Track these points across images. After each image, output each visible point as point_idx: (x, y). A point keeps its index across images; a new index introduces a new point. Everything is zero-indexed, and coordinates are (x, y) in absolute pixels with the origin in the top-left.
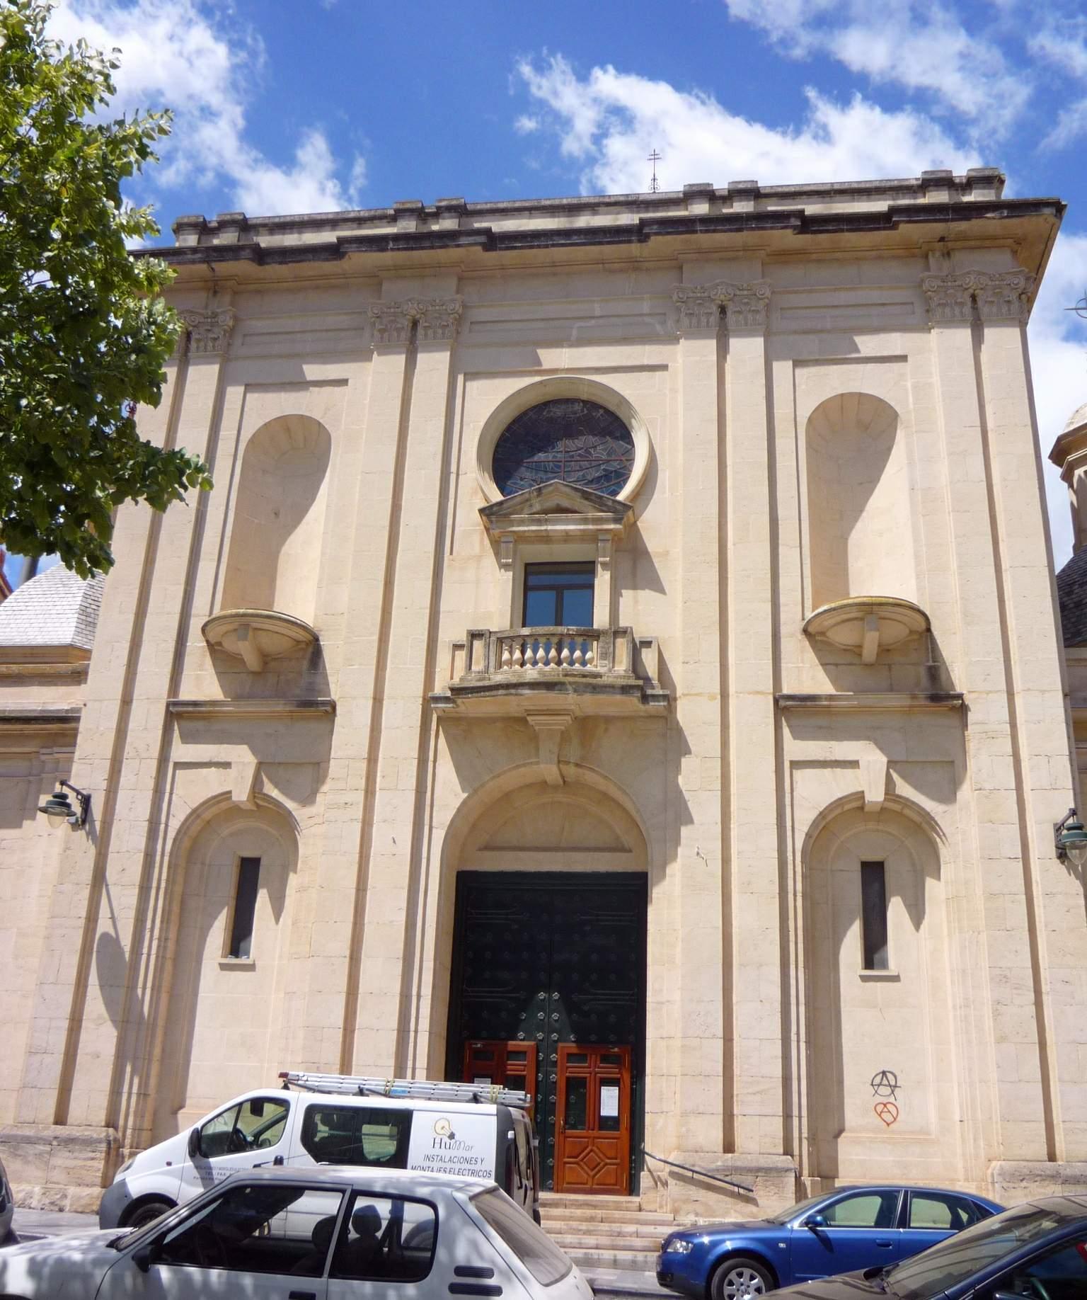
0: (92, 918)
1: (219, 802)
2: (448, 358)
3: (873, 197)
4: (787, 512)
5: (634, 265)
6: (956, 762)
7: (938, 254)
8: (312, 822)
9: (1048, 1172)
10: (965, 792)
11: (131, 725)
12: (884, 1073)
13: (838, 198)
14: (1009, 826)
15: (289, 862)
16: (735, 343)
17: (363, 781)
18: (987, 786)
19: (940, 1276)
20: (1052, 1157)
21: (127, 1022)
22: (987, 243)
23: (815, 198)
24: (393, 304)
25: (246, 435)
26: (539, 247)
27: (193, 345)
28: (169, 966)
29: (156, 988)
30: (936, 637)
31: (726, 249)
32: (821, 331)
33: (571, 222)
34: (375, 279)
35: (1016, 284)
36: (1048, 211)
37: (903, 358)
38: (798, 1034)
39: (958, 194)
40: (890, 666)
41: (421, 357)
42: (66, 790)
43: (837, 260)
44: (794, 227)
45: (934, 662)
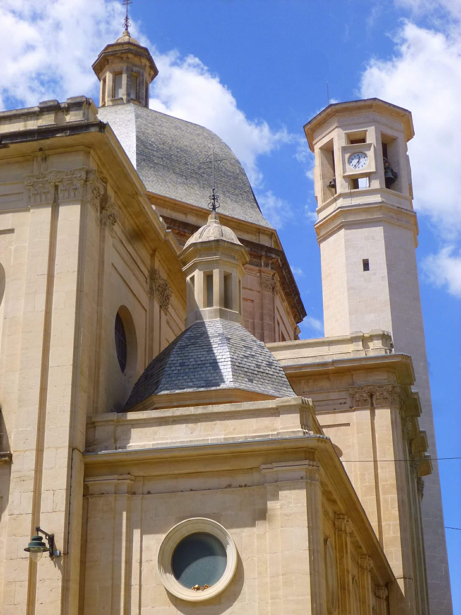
3: (12, 121)
6: (4, 497)
7: (39, 159)
14: (24, 537)
16: (63, 210)
22: (69, 149)
24: (69, 172)
27: (61, 195)
30: (4, 416)
35: (80, 177)
36: (93, 130)
37: (11, 231)
39: (63, 115)
42: (40, 534)
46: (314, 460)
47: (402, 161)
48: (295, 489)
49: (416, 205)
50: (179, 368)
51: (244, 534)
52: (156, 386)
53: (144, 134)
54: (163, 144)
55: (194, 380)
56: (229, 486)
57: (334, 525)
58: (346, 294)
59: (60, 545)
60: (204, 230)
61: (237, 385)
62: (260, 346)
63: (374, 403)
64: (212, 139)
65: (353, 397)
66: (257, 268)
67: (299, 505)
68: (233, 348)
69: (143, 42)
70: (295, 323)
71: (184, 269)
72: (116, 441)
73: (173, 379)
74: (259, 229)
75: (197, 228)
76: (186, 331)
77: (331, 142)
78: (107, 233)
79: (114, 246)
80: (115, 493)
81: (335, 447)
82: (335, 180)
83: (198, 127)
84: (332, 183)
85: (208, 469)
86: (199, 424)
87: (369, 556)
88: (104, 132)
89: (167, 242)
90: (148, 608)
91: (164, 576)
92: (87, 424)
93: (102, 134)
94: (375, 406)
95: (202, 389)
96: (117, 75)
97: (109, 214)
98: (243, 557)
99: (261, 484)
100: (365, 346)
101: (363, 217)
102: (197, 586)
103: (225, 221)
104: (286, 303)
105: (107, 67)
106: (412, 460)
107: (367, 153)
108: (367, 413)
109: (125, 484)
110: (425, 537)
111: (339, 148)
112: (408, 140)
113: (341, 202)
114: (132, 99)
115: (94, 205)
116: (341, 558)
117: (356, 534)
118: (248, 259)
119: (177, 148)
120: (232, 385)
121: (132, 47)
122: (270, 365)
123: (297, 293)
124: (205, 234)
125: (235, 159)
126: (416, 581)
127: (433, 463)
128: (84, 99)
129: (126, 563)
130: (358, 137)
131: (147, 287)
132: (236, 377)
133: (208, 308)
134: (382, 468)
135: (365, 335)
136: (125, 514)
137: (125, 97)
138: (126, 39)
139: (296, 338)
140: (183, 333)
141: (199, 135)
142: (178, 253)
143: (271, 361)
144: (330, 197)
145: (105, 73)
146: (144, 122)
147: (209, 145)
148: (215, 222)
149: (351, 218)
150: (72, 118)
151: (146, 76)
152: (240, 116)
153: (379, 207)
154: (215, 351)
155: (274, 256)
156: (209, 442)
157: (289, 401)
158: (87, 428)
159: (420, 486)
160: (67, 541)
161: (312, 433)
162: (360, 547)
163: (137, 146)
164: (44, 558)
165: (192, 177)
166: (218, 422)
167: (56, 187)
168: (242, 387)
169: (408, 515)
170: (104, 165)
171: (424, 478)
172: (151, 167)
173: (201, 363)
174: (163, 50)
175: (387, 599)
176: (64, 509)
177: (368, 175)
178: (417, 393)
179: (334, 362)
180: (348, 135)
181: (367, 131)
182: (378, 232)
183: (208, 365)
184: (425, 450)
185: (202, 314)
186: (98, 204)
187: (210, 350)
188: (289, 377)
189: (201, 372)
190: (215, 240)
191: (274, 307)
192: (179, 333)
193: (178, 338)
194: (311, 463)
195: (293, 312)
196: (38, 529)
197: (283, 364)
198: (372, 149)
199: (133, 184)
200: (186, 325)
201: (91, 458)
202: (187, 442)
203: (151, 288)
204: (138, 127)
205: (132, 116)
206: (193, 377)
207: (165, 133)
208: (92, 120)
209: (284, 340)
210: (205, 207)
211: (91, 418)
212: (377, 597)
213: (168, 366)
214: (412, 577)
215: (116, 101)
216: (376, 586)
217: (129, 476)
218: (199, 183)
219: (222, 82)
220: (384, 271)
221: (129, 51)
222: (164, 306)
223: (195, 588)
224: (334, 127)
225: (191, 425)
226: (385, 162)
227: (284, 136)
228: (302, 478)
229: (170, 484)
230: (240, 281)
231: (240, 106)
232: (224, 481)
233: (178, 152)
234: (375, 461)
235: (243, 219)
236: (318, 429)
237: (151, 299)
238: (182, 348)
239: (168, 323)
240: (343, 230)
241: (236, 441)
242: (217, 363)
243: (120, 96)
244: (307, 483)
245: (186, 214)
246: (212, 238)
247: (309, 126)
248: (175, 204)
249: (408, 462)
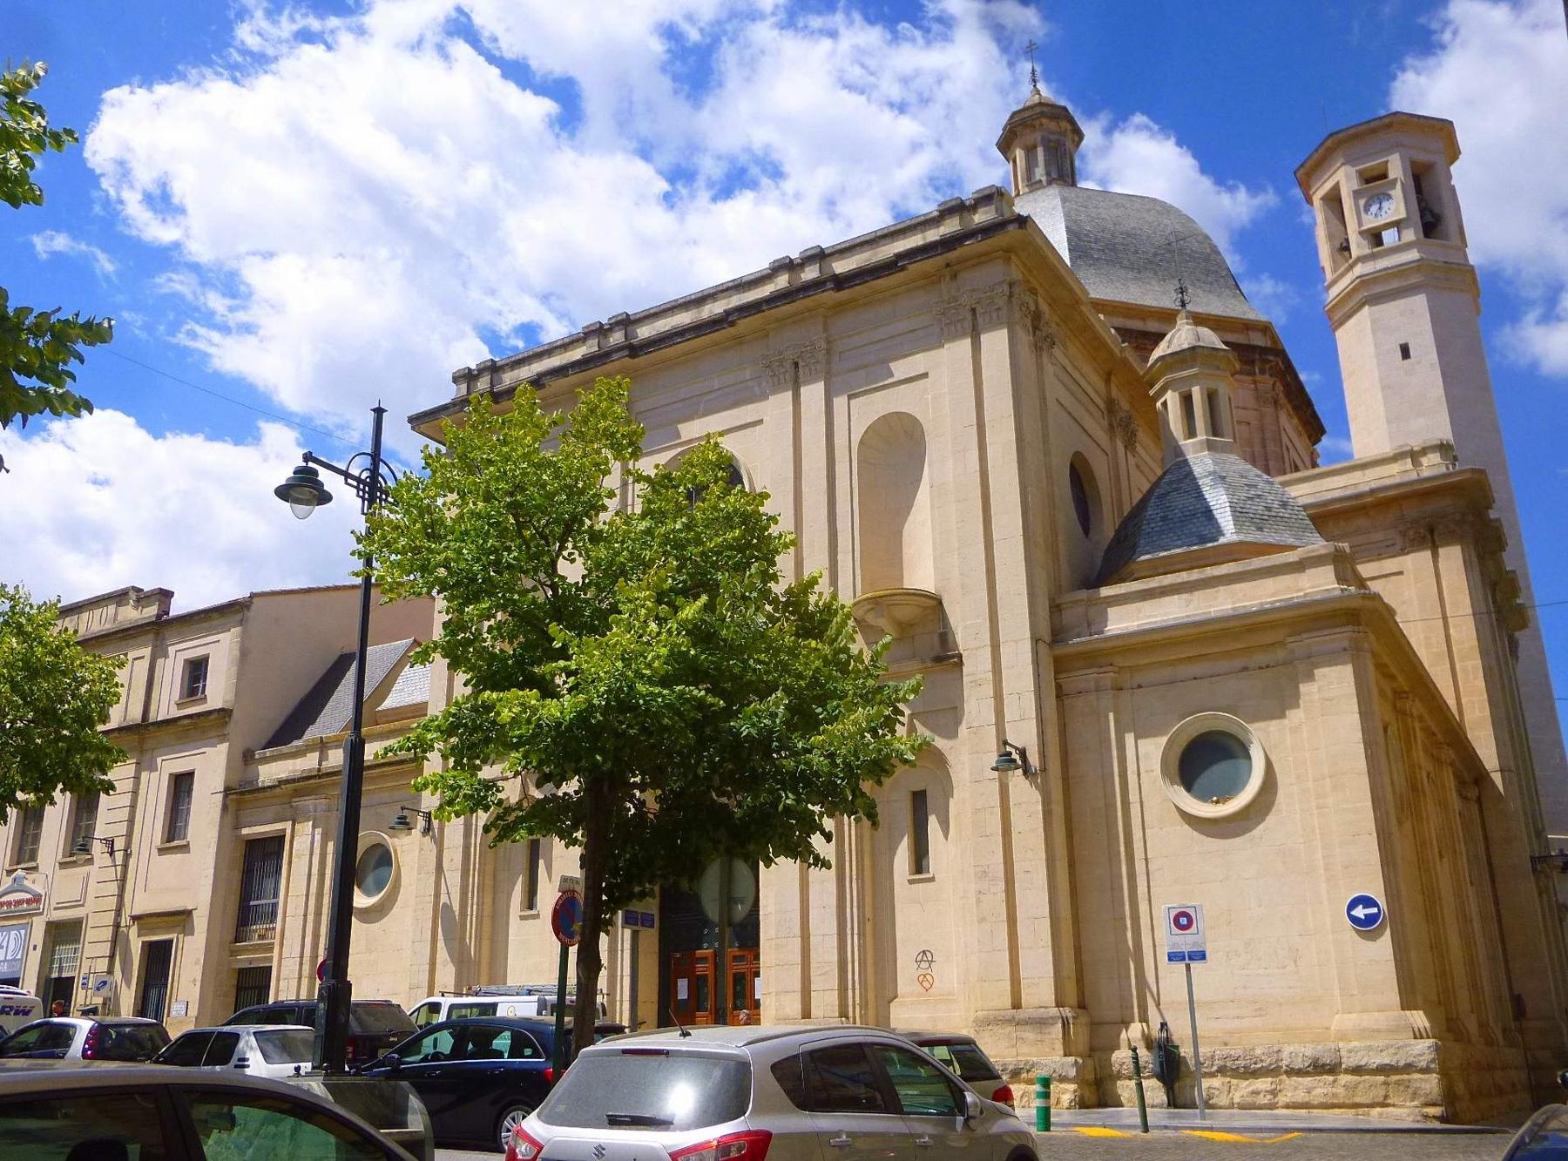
0: (437, 895)
2: (791, 398)
4: (843, 524)
5: (739, 341)
9: (1007, 1018)
10: (963, 730)
12: (924, 952)
13: (883, 242)
15: (947, 791)
16: (985, 338)
18: (975, 724)
20: (1016, 1005)
21: (462, 962)
23: (866, 247)
25: (856, 439)
26: (666, 347)
27: (980, 320)
28: (487, 921)
29: (479, 938)
31: (796, 314)
32: (866, 366)
34: (763, 334)
36: (1011, 228)
37: (925, 375)
38: (852, 929)
40: (913, 637)
41: (984, 338)
42: (1009, 749)
43: (879, 300)
44: (832, 289)
46: (1359, 624)
47: (1445, 194)
48: (1337, 665)
49: (1473, 258)
50: (1161, 523)
51: (1272, 729)
52: (1133, 550)
54: (1103, 231)
56: (1245, 669)
57: (1395, 707)
58: (1380, 396)
59: (1034, 760)
60: (1173, 336)
61: (1242, 537)
62: (1268, 482)
65: (1405, 536)
66: (1249, 378)
68: (1231, 489)
69: (1062, 102)
71: (1151, 393)
72: (1089, 625)
74: (1245, 324)
75: (1162, 336)
76: (1164, 474)
77: (1336, 188)
78: (1045, 360)
79: (1056, 376)
80: (1097, 691)
81: (1387, 606)
82: (1347, 240)
84: (1344, 245)
85: (1216, 650)
86: (1196, 593)
87: (1448, 745)
88: (1026, 228)
89: (1125, 361)
91: (1171, 788)
93: (1024, 231)
94: (1438, 543)
95: (1196, 548)
96: (1030, 151)
97: (1044, 334)
98: (1273, 758)
99: (1287, 663)
100: (1416, 463)
101: (1395, 284)
102: (1215, 798)
103: (1199, 320)
104: (1295, 421)
105: (1016, 142)
106: (1498, 612)
107: (1392, 193)
108: (1428, 554)
109: (1108, 678)
110: (1527, 714)
111: (1349, 194)
112: (1452, 163)
113: (1359, 270)
114: (1054, 179)
115: (1025, 326)
116: (1409, 751)
117: (1427, 717)
118: (1238, 366)
119: (1122, 234)
120: (1235, 538)
121: (1045, 109)
122: (1284, 505)
123: (1309, 404)
124: (1175, 341)
125: (1202, 234)
126: (1519, 774)
127: (1530, 612)
128: (994, 190)
129: (1120, 776)
130: (1376, 173)
131: (1105, 423)
134: (1455, 626)
135: (1415, 449)
136: (1111, 716)
137: (1044, 179)
139: (1315, 465)
140: (1160, 478)
141: (1149, 210)
142: (1141, 374)
145: (1014, 151)
146: (1074, 206)
147: (1166, 221)
148: (1187, 324)
149: (1378, 289)
150: (981, 217)
151: (1069, 144)
152: (1206, 183)
153: (1417, 266)
154: (1207, 496)
155: (1271, 358)
156: (1213, 615)
157: (1317, 550)
158: (1051, 612)
159: (1513, 646)
160: (1043, 755)
161: (1352, 588)
162: (1434, 734)
163: (1068, 240)
164: (1016, 778)
165: (1147, 269)
166: (1221, 588)
167: (973, 310)
168: (1249, 539)
169: (1499, 687)
170: (1030, 271)
171: (1517, 634)
172: (1090, 266)
174: (1091, 114)
175: (1479, 800)
176: (1034, 716)
177: (1397, 224)
178: (1498, 520)
179: (1372, 491)
180: (1360, 173)
181: (1387, 162)
182: (1420, 302)
184: (1516, 596)
185: (1183, 448)
186: (1029, 324)
187: (1200, 496)
188: (1313, 518)
189: (1191, 526)
190: (1189, 348)
191: (1279, 427)
192: (1154, 479)
193: (1155, 485)
194: (1356, 628)
195: (1307, 431)
196: (1005, 743)
197: (1301, 501)
198: (1399, 185)
199: (1071, 291)
200: (1162, 468)
201: (1061, 650)
202: (1183, 617)
203: (1111, 425)
204: (1067, 215)
205: (1058, 201)
207: (1103, 216)
208: (1007, 215)
209: (1297, 469)
210: (1169, 306)
212: (1463, 798)
214: (1513, 768)
215: (1033, 185)
216: (1461, 783)
217: (1111, 668)
218: (1156, 273)
219: (1179, 144)
221: (1042, 115)
222: (1130, 445)
223: (1212, 802)
224: (1339, 165)
225: (1184, 596)
226: (1420, 201)
227: (1270, 198)
228: (1345, 650)
229: (1166, 673)
230: (1230, 399)
231: (1203, 170)
232: (1238, 663)
234: (1445, 618)
235: (1224, 314)
236: (1361, 583)
237: (1112, 439)
238: (1162, 497)
239: (1138, 467)
240: (1367, 307)
241: (1248, 610)
242: (1211, 511)
243: (1038, 178)
244: (1352, 655)
245: (1144, 319)
246: (1186, 346)
247: (1302, 171)
248: (1129, 309)
249: (1493, 615)
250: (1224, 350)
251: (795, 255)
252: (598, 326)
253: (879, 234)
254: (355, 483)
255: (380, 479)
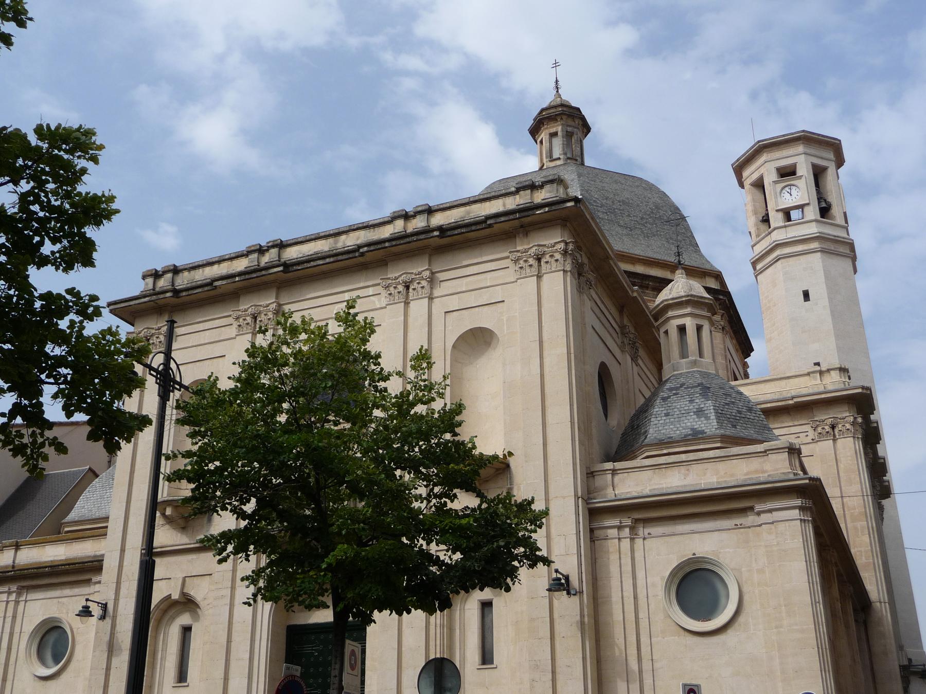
1: (158, 607)
8: (208, 607)
11: (125, 564)
17: (230, 583)
19: (617, 653)
33: (336, 243)
42: (89, 604)
45: (510, 485)
50: (664, 418)
53: (587, 191)
54: (606, 199)
55: (681, 429)
63: (837, 434)
64: (651, 189)
65: (814, 430)
67: (796, 540)
70: (743, 358)
73: (660, 428)
83: (636, 179)
90: (659, 639)
92: (587, 474)
94: (837, 437)
104: (734, 341)
119: (619, 201)
130: (788, 171)
131: (619, 342)
132: (721, 424)
133: (684, 360)
138: (558, 101)
141: (638, 186)
143: (750, 406)
144: (764, 232)
147: (649, 195)
153: (819, 238)
173: (684, 412)
183: (692, 414)
189: (686, 421)
206: (679, 426)
207: (606, 189)
211: (589, 468)
213: (653, 416)
220: (825, 302)
233: (621, 205)
250: (709, 299)
251: (409, 209)
252: (258, 247)
253: (471, 200)
254: (155, 374)
255: (170, 371)
